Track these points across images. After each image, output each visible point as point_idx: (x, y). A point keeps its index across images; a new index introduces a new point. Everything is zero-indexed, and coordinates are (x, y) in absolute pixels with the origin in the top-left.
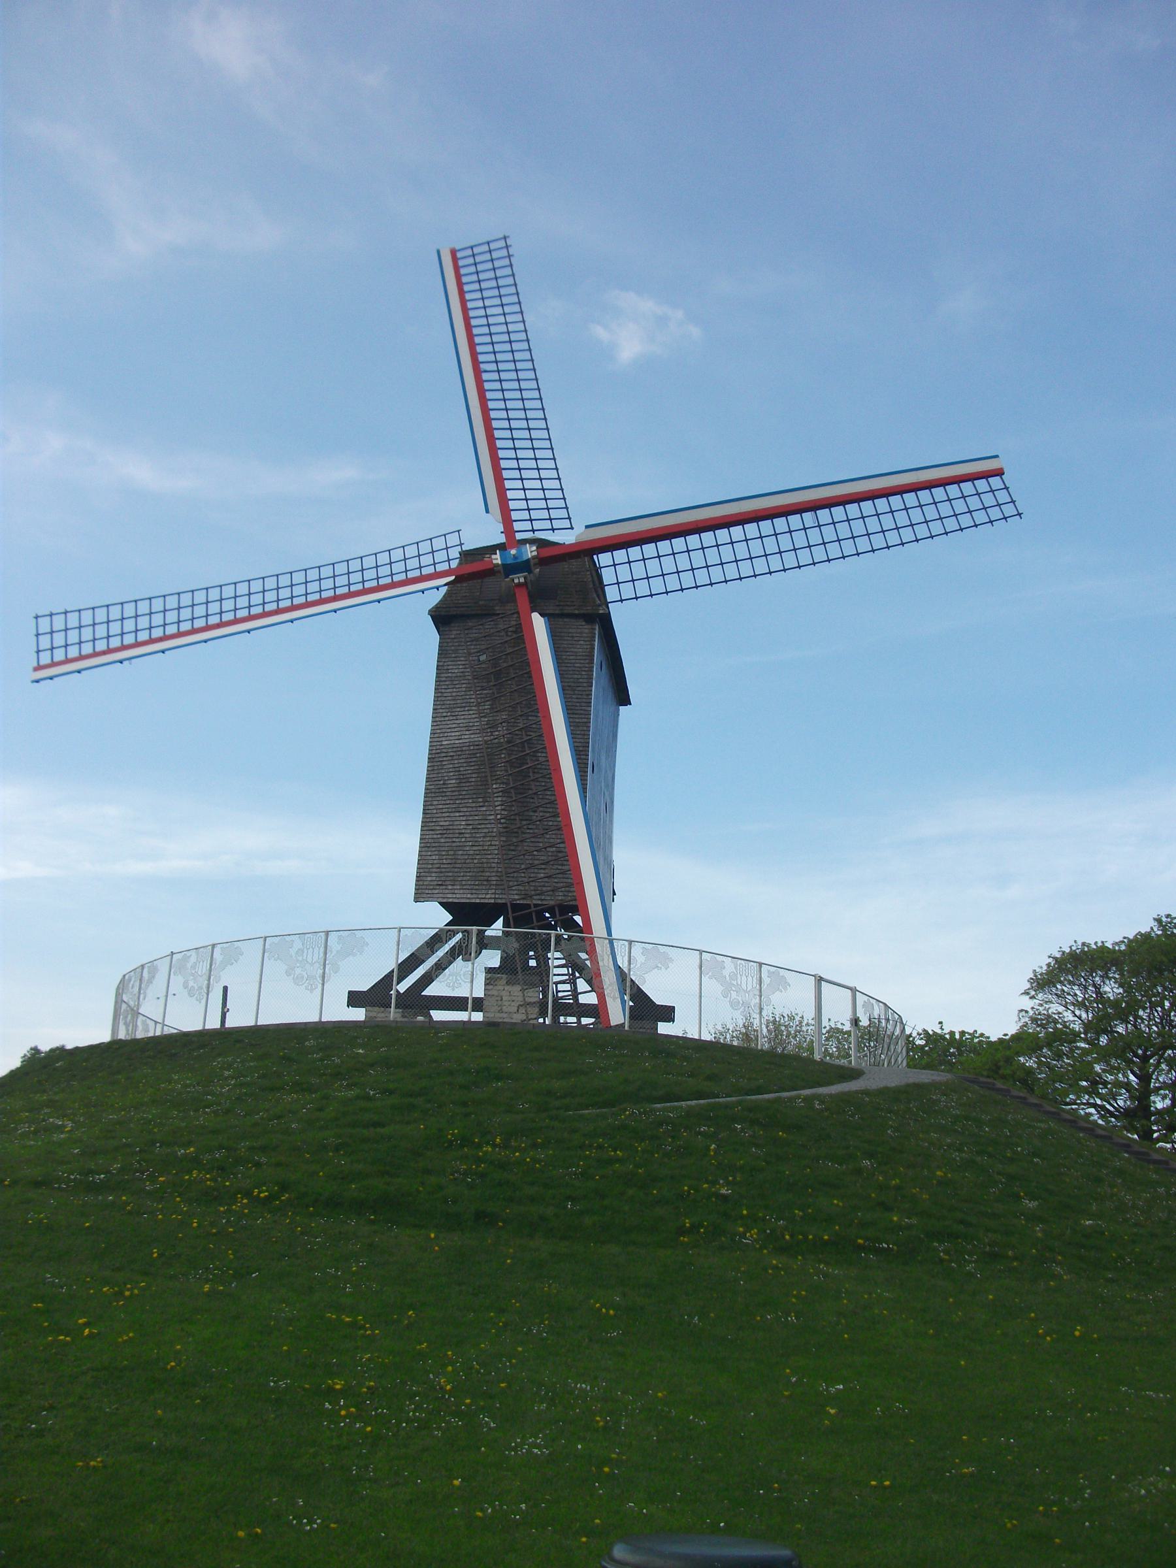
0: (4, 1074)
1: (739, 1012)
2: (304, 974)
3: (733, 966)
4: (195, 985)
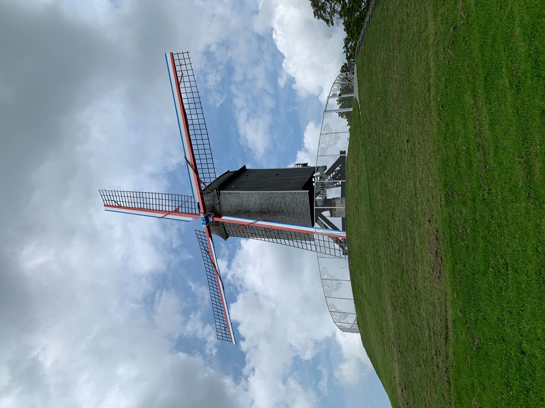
1: (338, 141)
2: (336, 286)
3: (322, 145)
4: (343, 316)
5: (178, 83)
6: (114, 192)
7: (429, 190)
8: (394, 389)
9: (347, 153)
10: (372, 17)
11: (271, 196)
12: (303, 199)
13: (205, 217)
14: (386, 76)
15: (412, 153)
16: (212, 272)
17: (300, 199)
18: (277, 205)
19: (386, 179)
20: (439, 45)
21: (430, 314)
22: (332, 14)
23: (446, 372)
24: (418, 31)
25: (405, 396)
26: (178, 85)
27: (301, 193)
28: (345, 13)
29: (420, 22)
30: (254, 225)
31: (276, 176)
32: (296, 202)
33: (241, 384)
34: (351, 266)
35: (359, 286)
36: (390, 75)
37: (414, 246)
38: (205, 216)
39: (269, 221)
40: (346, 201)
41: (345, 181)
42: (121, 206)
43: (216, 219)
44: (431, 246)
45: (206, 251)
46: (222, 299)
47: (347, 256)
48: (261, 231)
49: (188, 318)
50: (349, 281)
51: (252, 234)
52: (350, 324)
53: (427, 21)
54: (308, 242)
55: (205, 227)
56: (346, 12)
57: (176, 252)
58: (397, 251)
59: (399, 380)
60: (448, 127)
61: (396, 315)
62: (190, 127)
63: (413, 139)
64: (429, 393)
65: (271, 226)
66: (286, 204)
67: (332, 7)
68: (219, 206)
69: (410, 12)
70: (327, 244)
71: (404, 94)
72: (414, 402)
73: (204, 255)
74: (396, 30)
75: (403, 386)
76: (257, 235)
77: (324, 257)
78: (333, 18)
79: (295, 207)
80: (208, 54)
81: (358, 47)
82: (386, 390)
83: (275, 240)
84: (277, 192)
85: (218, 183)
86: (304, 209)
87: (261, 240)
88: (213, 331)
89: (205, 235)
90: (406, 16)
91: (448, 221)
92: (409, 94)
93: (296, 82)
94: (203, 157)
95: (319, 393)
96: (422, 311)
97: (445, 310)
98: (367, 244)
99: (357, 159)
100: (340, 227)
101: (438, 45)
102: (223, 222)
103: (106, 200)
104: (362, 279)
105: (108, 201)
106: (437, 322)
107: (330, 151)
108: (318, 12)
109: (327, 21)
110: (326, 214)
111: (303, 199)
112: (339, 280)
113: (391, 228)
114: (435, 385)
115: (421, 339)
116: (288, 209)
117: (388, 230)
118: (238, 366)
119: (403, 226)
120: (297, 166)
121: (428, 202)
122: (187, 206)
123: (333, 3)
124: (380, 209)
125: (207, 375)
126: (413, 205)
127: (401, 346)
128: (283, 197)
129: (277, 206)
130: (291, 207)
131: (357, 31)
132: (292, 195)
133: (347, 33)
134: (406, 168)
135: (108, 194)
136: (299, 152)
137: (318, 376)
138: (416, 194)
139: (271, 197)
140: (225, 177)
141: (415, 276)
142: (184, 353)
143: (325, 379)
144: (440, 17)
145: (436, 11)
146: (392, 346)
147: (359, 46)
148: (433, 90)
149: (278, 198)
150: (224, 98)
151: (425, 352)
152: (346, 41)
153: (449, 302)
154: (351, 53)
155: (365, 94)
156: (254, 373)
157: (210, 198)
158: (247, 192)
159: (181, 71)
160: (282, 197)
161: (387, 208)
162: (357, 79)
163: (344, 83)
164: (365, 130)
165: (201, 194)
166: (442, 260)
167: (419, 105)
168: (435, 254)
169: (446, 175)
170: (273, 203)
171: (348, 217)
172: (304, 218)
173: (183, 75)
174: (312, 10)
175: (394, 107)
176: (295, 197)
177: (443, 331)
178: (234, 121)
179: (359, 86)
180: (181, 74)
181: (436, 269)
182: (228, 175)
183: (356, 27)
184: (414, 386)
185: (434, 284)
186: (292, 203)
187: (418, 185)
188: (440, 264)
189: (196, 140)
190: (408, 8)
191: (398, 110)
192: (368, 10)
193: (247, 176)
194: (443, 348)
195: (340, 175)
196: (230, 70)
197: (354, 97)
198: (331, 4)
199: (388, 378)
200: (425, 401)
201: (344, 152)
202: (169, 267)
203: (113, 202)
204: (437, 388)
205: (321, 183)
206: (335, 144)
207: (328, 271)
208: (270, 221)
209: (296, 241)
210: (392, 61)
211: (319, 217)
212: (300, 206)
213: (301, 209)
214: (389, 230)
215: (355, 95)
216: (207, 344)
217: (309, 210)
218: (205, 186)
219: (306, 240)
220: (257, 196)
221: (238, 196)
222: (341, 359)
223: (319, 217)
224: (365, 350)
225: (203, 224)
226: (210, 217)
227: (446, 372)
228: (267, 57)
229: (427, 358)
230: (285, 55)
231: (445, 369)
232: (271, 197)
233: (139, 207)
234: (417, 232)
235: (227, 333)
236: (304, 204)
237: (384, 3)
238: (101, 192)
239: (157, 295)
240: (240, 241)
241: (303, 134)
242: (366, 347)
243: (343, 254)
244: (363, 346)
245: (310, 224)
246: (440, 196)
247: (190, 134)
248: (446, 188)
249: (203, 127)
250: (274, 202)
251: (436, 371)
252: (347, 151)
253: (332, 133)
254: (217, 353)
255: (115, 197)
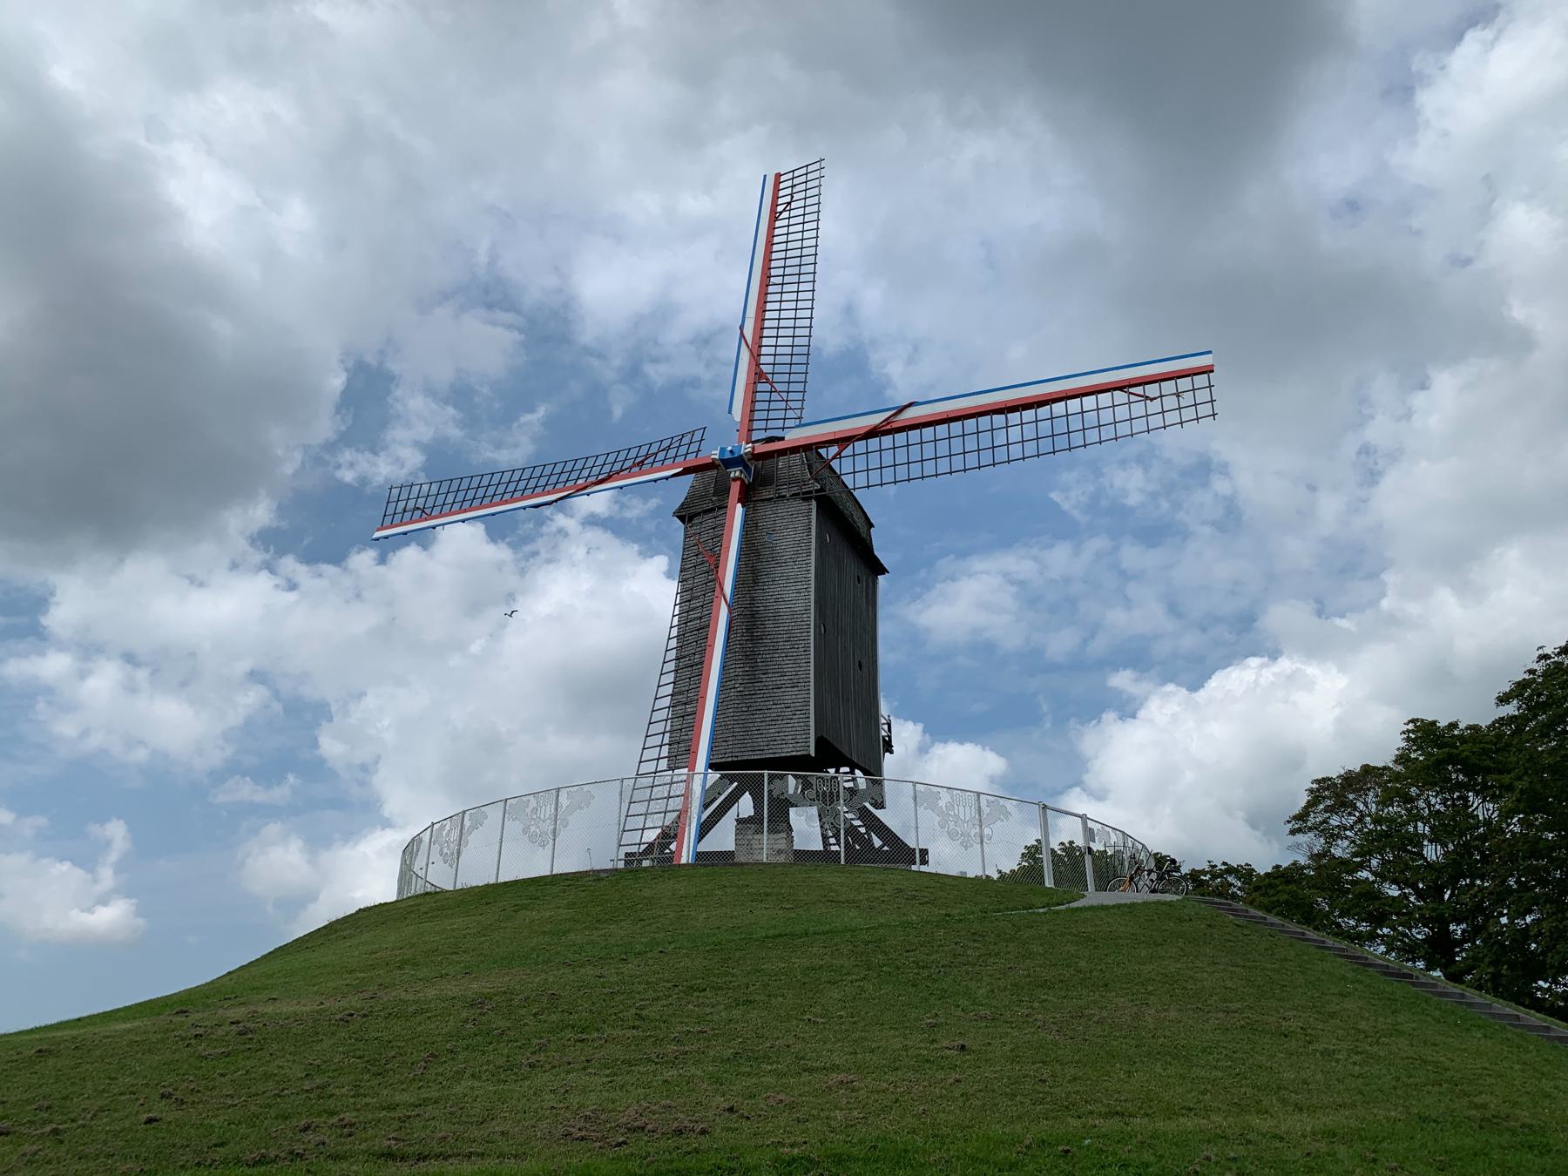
0: (12, 1028)
3: (949, 797)
5: (1125, 387)
6: (815, 200)
7: (822, 1110)
8: (235, 997)
9: (924, 868)
10: (1318, 947)
11: (800, 646)
12: (791, 737)
13: (741, 456)
14: (1151, 988)
15: (927, 1061)
16: (585, 473)
17: (790, 729)
18: (774, 663)
19: (852, 982)
20: (1246, 1145)
21: (461, 1109)
22: (1322, 830)
23: (291, 1153)
24: (1284, 1083)
25: (220, 1032)
26: (1121, 387)
27: (808, 732)
28: (1327, 869)
29: (1309, 1091)
30: (716, 595)
31: (857, 664)
32: (781, 718)
33: (251, 550)
34: (595, 876)
35: (538, 898)
36: (1152, 998)
37: (657, 1063)
38: (746, 458)
39: (728, 639)
40: (783, 865)
41: (842, 862)
42: (777, 219)
43: (735, 488)
44: (660, 1113)
45: (643, 458)
46: (507, 502)
47: (621, 865)
48: (699, 615)
49: (446, 402)
50: (552, 871)
51: (692, 589)
52: (424, 870)
53: (1314, 1111)
54: (665, 751)
55: (712, 457)
56: (1328, 873)
57: (633, 372)
58: (644, 1013)
59: (266, 1013)
60: (1007, 1167)
61: (456, 1008)
62: (999, 419)
63: (968, 1064)
64: (230, 1102)
65: (712, 646)
66: (775, 691)
67: (1344, 831)
68: (771, 496)
69: (1337, 1061)
70: (655, 806)
71: (1099, 1040)
72: (203, 1057)
73: (633, 454)
74: (1284, 1019)
75: (248, 1025)
76: (688, 604)
77: (621, 799)
78: (1311, 835)
79: (768, 715)
80: (1203, 469)
81: (1230, 905)
82: (229, 973)
83: (672, 655)
84: (812, 664)
85: (837, 494)
86: (761, 740)
87: (674, 616)
88: (405, 471)
89: (691, 457)
90: (1326, 1049)
91: (734, 1164)
92: (1098, 1054)
93: (1124, 721)
94: (915, 452)
95: (219, 777)
96: (470, 1084)
97: (471, 1153)
98: (659, 925)
99: (907, 899)
100: (709, 845)
101: (1244, 1142)
102: (727, 507)
103: (792, 179)
104: (559, 907)
105: (789, 183)
106: (436, 1128)
107: (928, 818)
108: (1328, 789)
109: (1302, 816)
110: (746, 805)
111: (791, 737)
112: (554, 840)
113: (709, 995)
114: (251, 1120)
115: (386, 1079)
116: (761, 696)
117: (705, 986)
118: (305, 542)
119: (716, 1032)
120: (884, 724)
121: (786, 1105)
122: (773, 405)
123: (1356, 834)
124: (764, 964)
125: (280, 452)
126: (778, 1063)
127: (364, 1020)
128: (795, 681)
129: (769, 663)
130: (768, 703)
131: (1273, 902)
132: (802, 708)
133: (1267, 874)
134: (883, 1044)
135: (810, 185)
136: (920, 727)
137: (267, 774)
138: (810, 1070)
139: (796, 646)
140: (856, 516)
141: (569, 1063)
142: (342, 388)
143: (260, 796)
144: (1325, 1150)
145: (1343, 1138)
146: (366, 995)
147: (1233, 910)
148: (1113, 1124)
149: (794, 666)
150: (1076, 513)
151: (347, 1090)
152: (1245, 869)
153: (496, 1164)
154: (1209, 886)
155: (1096, 925)
156: (283, 590)
157: (796, 471)
158: (813, 579)
159: (1161, 396)
160: (797, 677)
161: (766, 986)
162: (1140, 901)
163: (1126, 863)
164: (993, 925)
165: (809, 448)
166: (619, 1145)
167: (1069, 1082)
168: (636, 1124)
169: (866, 1161)
170: (779, 651)
171: (737, 870)
172: (737, 742)
173: (1148, 402)
174: (1334, 772)
175: (1061, 1008)
176: (796, 717)
177: (410, 1145)
178: (1005, 543)
179: (1119, 906)
180: (1152, 397)
181: (592, 1128)
182: (860, 523)
183: (1286, 902)
184: (248, 1058)
185: (548, 1121)
186: (778, 706)
187: (835, 1077)
188: (608, 1140)
189: (935, 440)
190: (1349, 1055)
191: (1051, 1020)
192: (1337, 935)
193: (858, 577)
194: (360, 1144)
195: (858, 848)
196: (1155, 533)
197: (1085, 893)
198: (1352, 828)
199: (270, 981)
200: (207, 1088)
201: (924, 862)
202: (587, 351)
203: (788, 199)
204: (244, 1126)
205: (838, 792)
206: (952, 835)
207: (580, 808)
208: (727, 642)
209: (670, 716)
210: (1194, 1006)
211: (736, 784)
212: (770, 731)
213: (761, 732)
214: (705, 990)
215: (1093, 897)
216: (368, 455)
217: (759, 757)
218: (830, 457)
219: (670, 745)
220: (800, 605)
221: (800, 552)
222: (318, 842)
223: (736, 784)
224: (347, 914)
225: (723, 450)
226: (741, 472)
227: (291, 1153)
228: (1190, 641)
229: (332, 1095)
230: (1201, 695)
231: (300, 1151)
232: (796, 646)
233: (773, 272)
234: (699, 1073)
235: (407, 516)
236: (775, 740)
237: (1361, 985)
238: (816, 166)
239: (510, 317)
240: (662, 554)
241: (972, 742)
242: (357, 916)
243: (627, 854)
244: (360, 909)
245: (716, 757)
246: (805, 1143)
247: (979, 419)
248: (830, 1160)
249: (986, 458)
250: (783, 655)
251: (294, 1122)
252: (928, 871)
253: (981, 826)
254: (343, 486)
255: (801, 203)
